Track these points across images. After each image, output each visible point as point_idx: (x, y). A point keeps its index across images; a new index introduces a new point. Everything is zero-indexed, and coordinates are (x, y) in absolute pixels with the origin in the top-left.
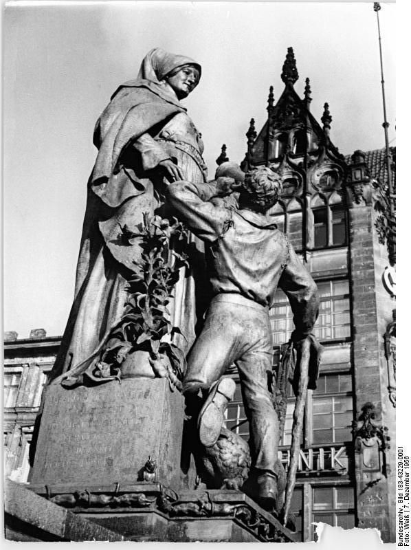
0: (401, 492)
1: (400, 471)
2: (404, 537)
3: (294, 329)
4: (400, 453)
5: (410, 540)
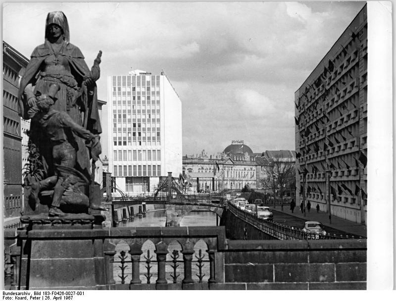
2: (9, 296)
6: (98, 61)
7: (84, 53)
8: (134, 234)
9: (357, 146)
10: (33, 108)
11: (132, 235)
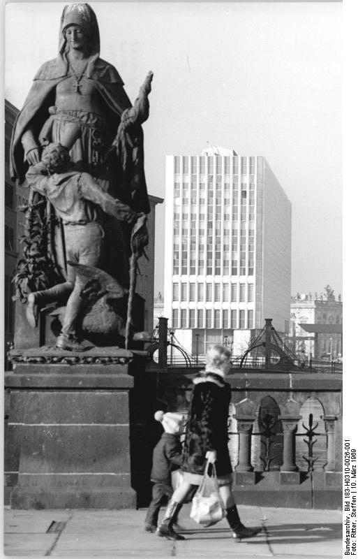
0: (347, 500)
1: (347, 458)
2: (351, 546)
3: (229, 444)
4: (347, 446)
5: (357, 548)
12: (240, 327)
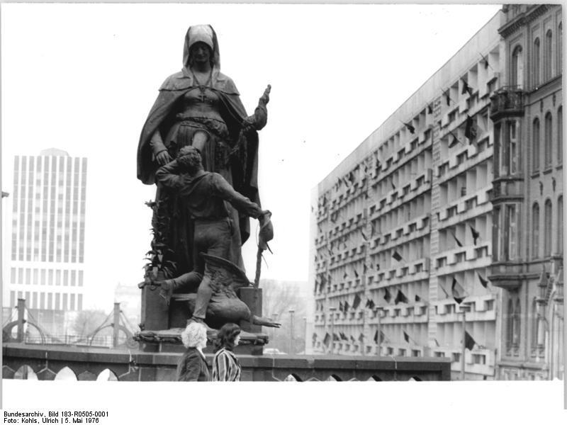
2: (13, 418)
6: (264, 100)
7: (240, 88)
8: (311, 365)
9: (426, 271)
10: (165, 166)
11: (310, 367)
12: (167, 298)
